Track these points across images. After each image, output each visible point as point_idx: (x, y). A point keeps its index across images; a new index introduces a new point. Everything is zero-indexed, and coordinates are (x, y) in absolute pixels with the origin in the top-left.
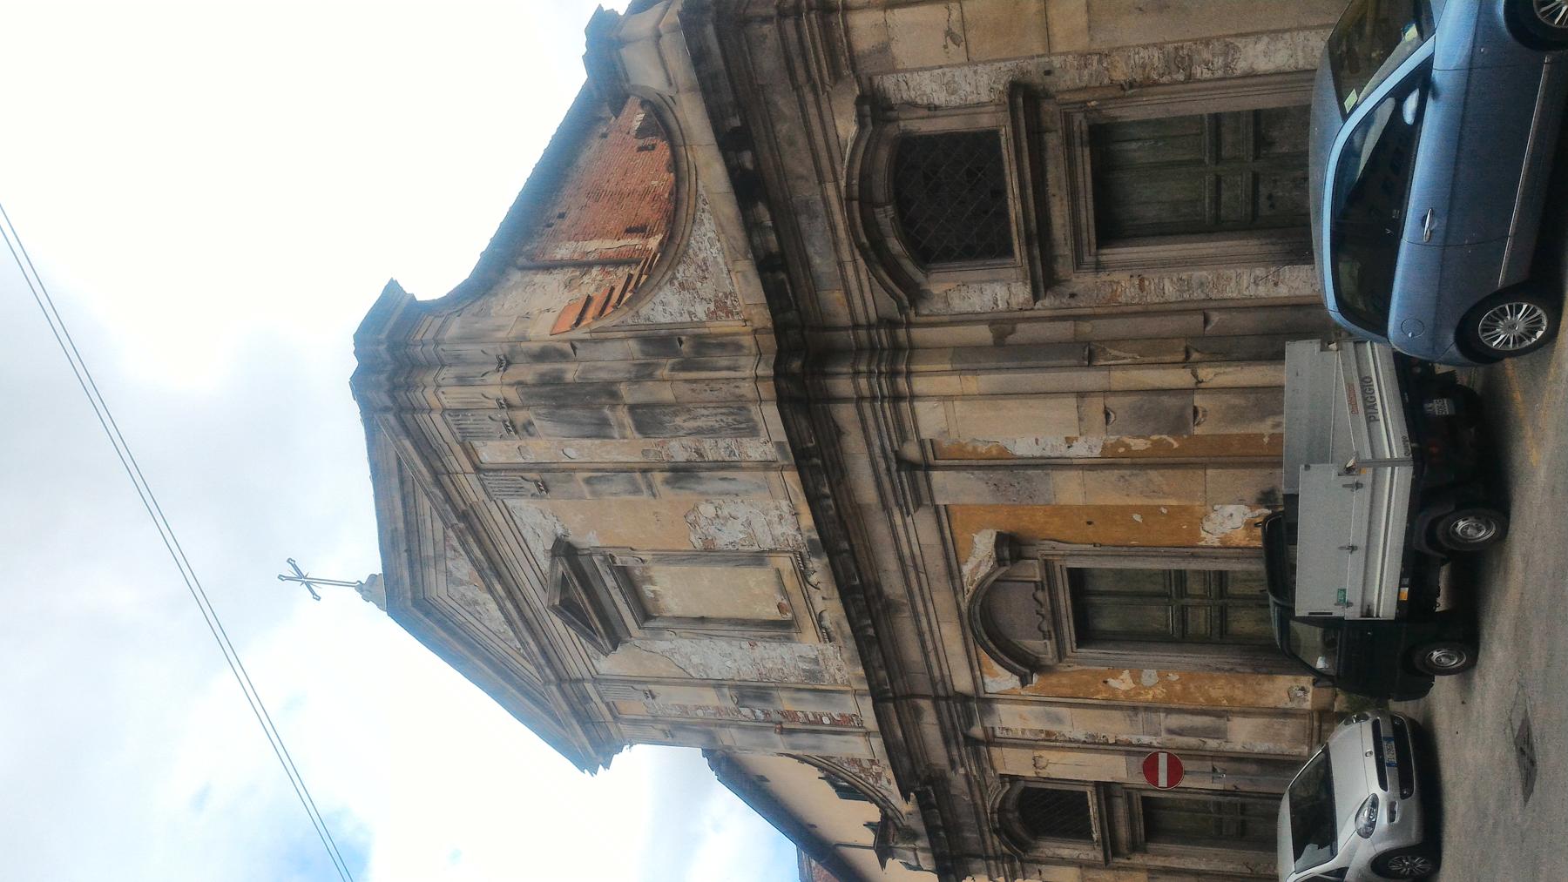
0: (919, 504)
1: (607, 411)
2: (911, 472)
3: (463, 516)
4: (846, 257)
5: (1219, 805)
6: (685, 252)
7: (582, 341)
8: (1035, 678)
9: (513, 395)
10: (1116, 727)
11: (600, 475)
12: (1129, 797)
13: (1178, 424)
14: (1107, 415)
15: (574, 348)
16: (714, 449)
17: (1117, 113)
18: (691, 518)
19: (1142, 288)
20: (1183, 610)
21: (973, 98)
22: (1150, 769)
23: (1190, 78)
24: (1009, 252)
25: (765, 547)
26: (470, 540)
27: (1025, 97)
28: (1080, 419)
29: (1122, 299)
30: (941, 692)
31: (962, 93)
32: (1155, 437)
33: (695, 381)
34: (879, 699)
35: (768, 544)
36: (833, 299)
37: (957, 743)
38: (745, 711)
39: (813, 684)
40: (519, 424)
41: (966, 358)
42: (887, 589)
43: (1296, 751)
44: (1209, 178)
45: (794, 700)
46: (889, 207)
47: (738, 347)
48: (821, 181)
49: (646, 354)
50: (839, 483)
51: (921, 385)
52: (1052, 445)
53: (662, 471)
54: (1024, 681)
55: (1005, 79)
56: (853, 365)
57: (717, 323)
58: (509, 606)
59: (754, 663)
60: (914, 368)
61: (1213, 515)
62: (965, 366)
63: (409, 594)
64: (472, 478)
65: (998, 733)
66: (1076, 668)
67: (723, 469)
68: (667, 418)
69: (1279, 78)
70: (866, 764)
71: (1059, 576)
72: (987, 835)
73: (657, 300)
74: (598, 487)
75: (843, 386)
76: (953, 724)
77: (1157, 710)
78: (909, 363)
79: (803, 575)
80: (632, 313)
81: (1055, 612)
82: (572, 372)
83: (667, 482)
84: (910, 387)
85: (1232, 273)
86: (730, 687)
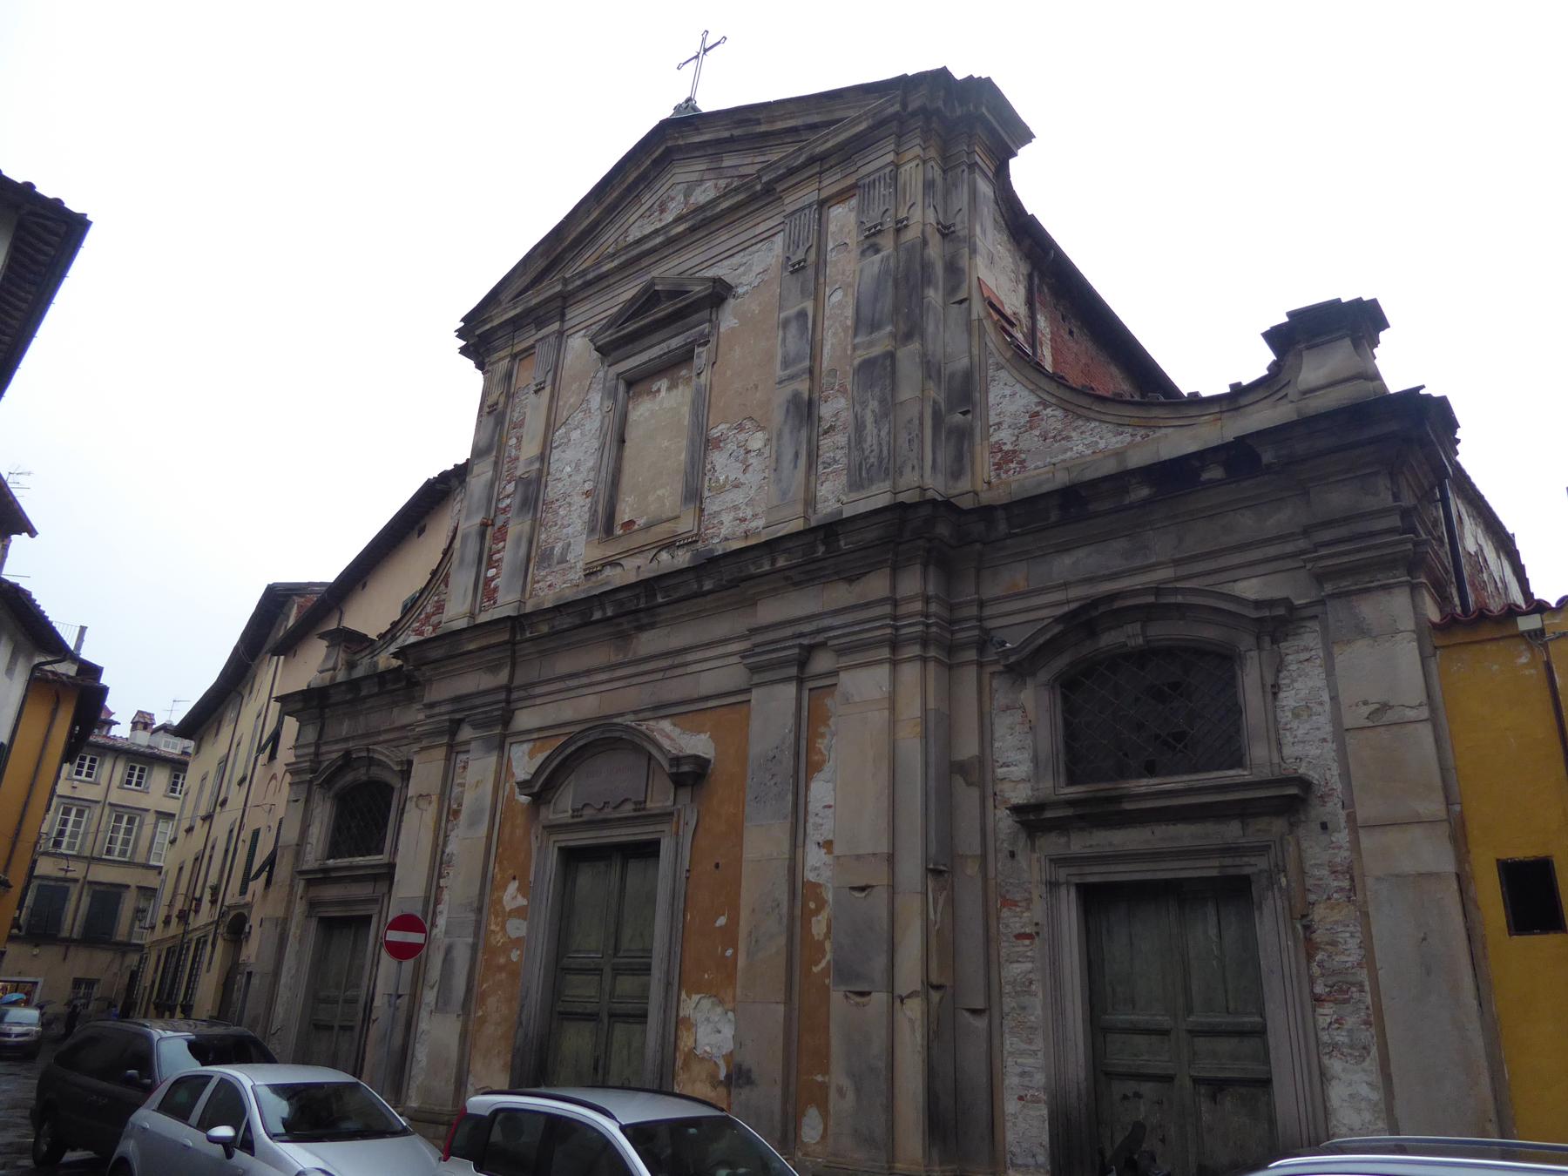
0: (754, 669)
1: (889, 328)
2: (798, 661)
3: (769, 190)
4: (1074, 592)
5: (354, 1001)
6: (1079, 417)
7: (969, 310)
8: (524, 799)
9: (912, 234)
10: (460, 887)
11: (807, 325)
12: (374, 901)
13: (844, 972)
14: (862, 889)
15: (961, 302)
16: (834, 447)
17: (1267, 909)
18: (748, 424)
19: (1020, 936)
20: (598, 971)
21: (1288, 738)
22: (407, 922)
23: (1318, 999)
24: (1072, 780)
25: (707, 504)
26: (741, 197)
27: (1291, 799)
28: (858, 857)
29: (1005, 913)
30: (515, 695)
31: (1295, 724)
32: (828, 946)
33: (921, 424)
34: (515, 622)
35: (711, 507)
36: (1017, 576)
37: (453, 712)
38: (510, 488)
39: (536, 556)
40: (879, 240)
41: (938, 728)
42: (645, 637)
43: (413, 1092)
44: (1164, 1021)
45: (519, 538)
46: (1140, 640)
47: (956, 475)
48: (1177, 562)
49: (952, 376)
50: (787, 578)
51: (910, 673)
52: (821, 824)
53: (811, 391)
54: (523, 785)
55: (1314, 776)
56: (937, 597)
57: (986, 455)
58: (658, 240)
59: (566, 495)
60: (931, 666)
61: (719, 1010)
62: (931, 725)
63: (681, 142)
64: (814, 197)
65: (462, 757)
66: (534, 846)
67: (809, 455)
68: (877, 390)
69: (1320, 1114)
70: (434, 619)
71: (651, 828)
72: (344, 746)
73: (1018, 387)
74: (793, 329)
75: (911, 584)
76: (477, 707)
77: (476, 935)
78: (937, 660)
79: (670, 545)
80: (1003, 361)
81: (605, 823)
82: (934, 296)
83: (796, 396)
84: (909, 660)
85: (1039, 1044)
86: (540, 470)
